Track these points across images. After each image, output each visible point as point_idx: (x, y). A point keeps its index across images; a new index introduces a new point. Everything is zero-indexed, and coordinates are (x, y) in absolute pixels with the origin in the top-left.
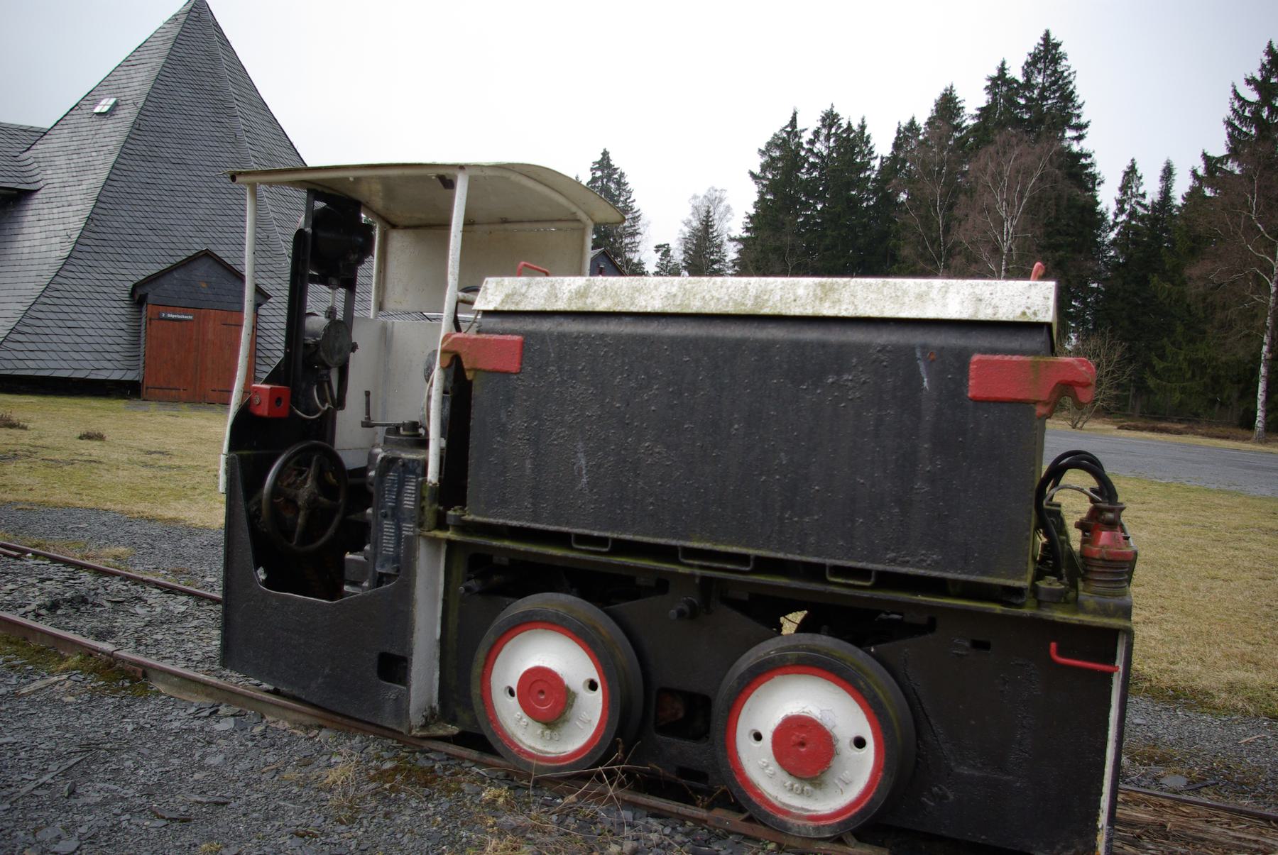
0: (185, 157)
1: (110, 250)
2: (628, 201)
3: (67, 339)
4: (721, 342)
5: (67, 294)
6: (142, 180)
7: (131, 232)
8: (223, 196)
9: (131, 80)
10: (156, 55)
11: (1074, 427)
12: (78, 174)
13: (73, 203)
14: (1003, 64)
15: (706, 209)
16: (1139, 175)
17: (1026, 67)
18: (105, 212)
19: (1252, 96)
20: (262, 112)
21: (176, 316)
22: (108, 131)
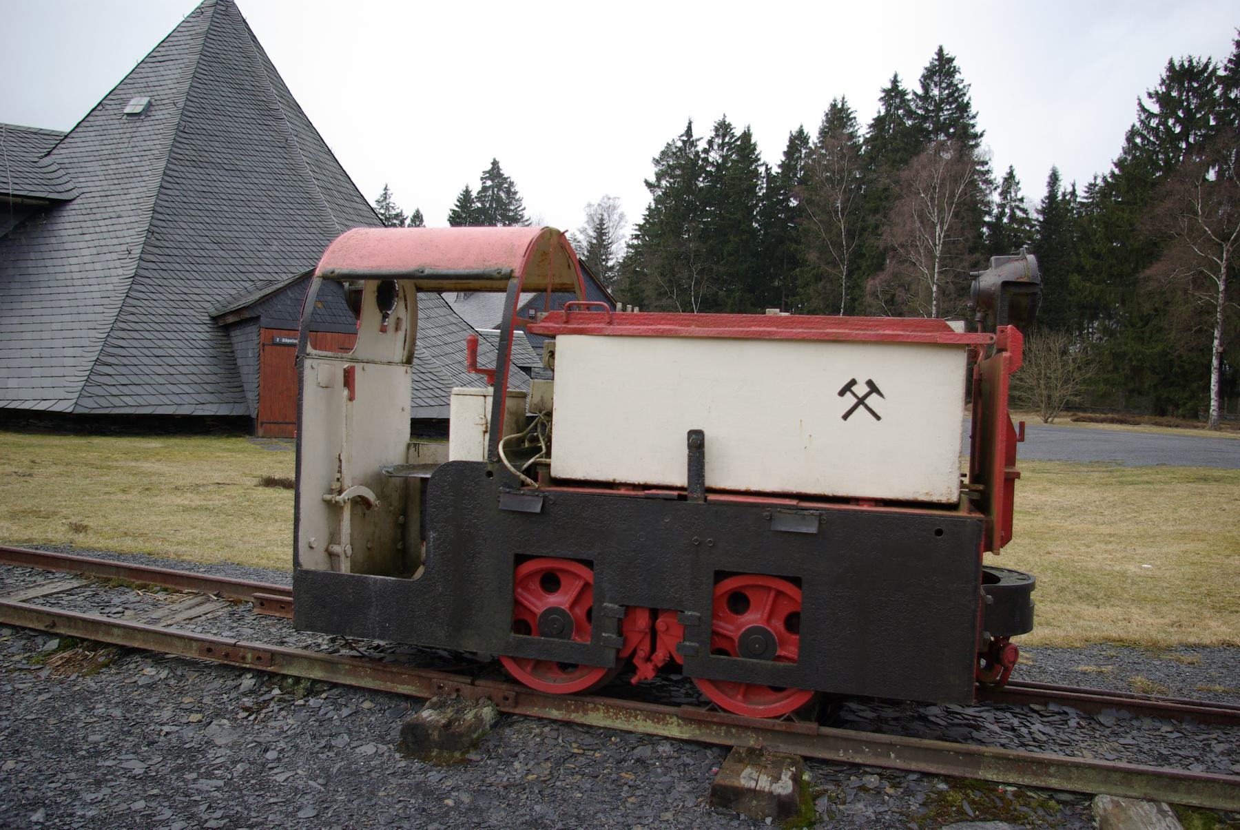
2: (519, 209)
3: (159, 370)
5: (144, 318)
6: (198, 189)
8: (285, 206)
9: (160, 78)
10: (187, 51)
11: (1046, 422)
13: (123, 214)
14: (896, 76)
15: (600, 217)
16: (1017, 181)
17: (922, 80)
18: (165, 225)
19: (1155, 108)
21: (291, 341)
22: (147, 133)
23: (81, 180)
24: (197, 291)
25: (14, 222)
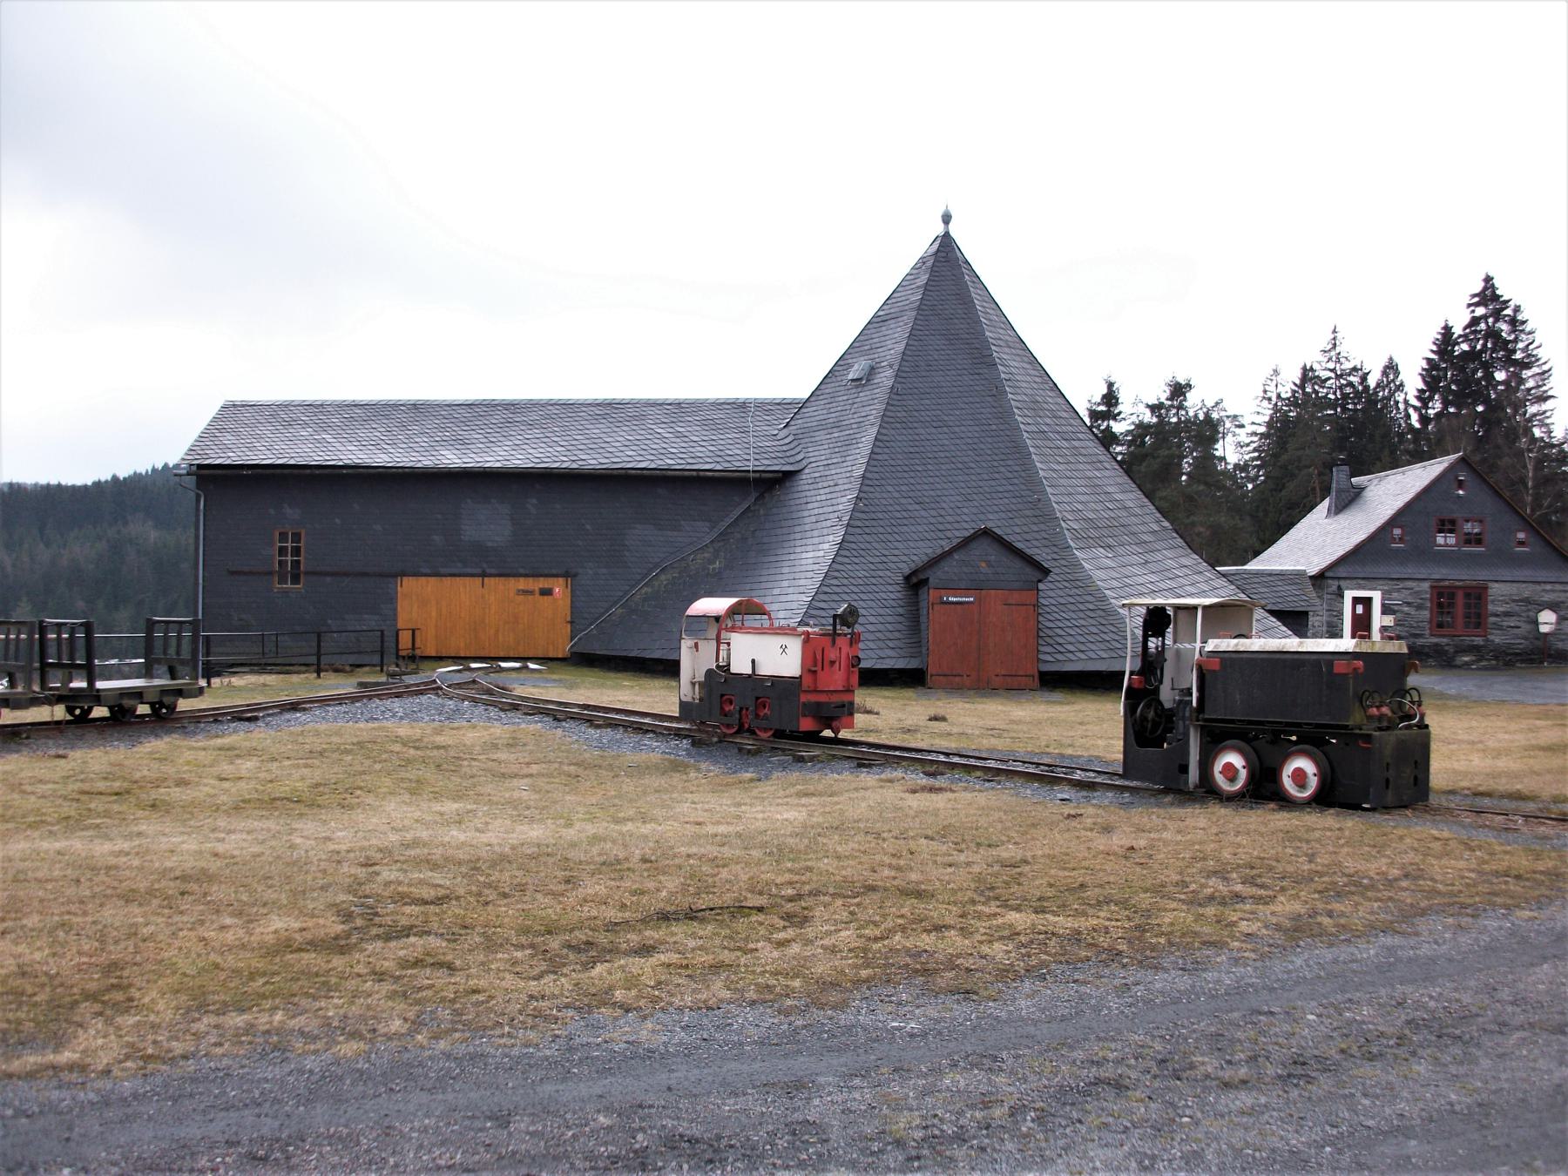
0: (946, 418)
1: (881, 530)
2: (1531, 347)
4: (1272, 659)
7: (898, 508)
8: (989, 458)
12: (841, 449)
13: (840, 482)
18: (872, 490)
22: (866, 399)
23: (810, 450)
24: (896, 552)
25: (754, 495)
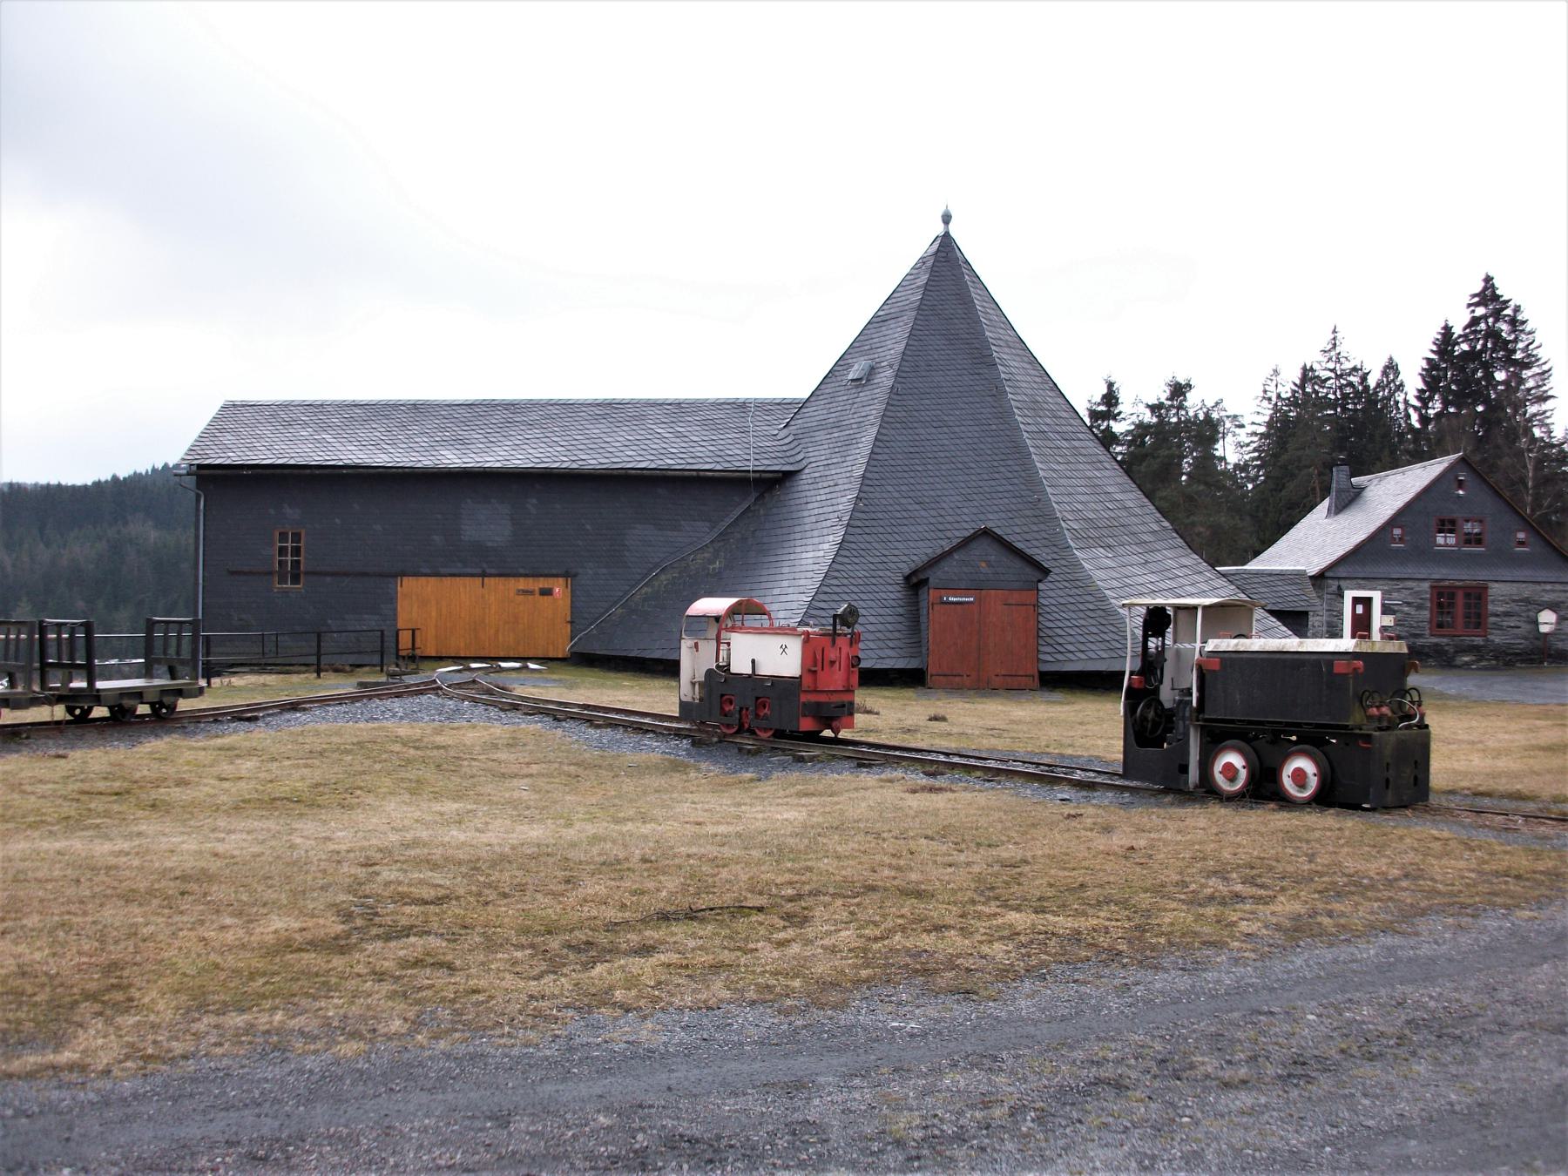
0: (946, 418)
2: (1531, 347)
4: (1272, 659)
7: (898, 508)
8: (989, 458)
12: (841, 449)
13: (840, 482)
18: (872, 490)
20: (1020, 352)
22: (866, 399)
24: (896, 552)
25: (754, 495)
